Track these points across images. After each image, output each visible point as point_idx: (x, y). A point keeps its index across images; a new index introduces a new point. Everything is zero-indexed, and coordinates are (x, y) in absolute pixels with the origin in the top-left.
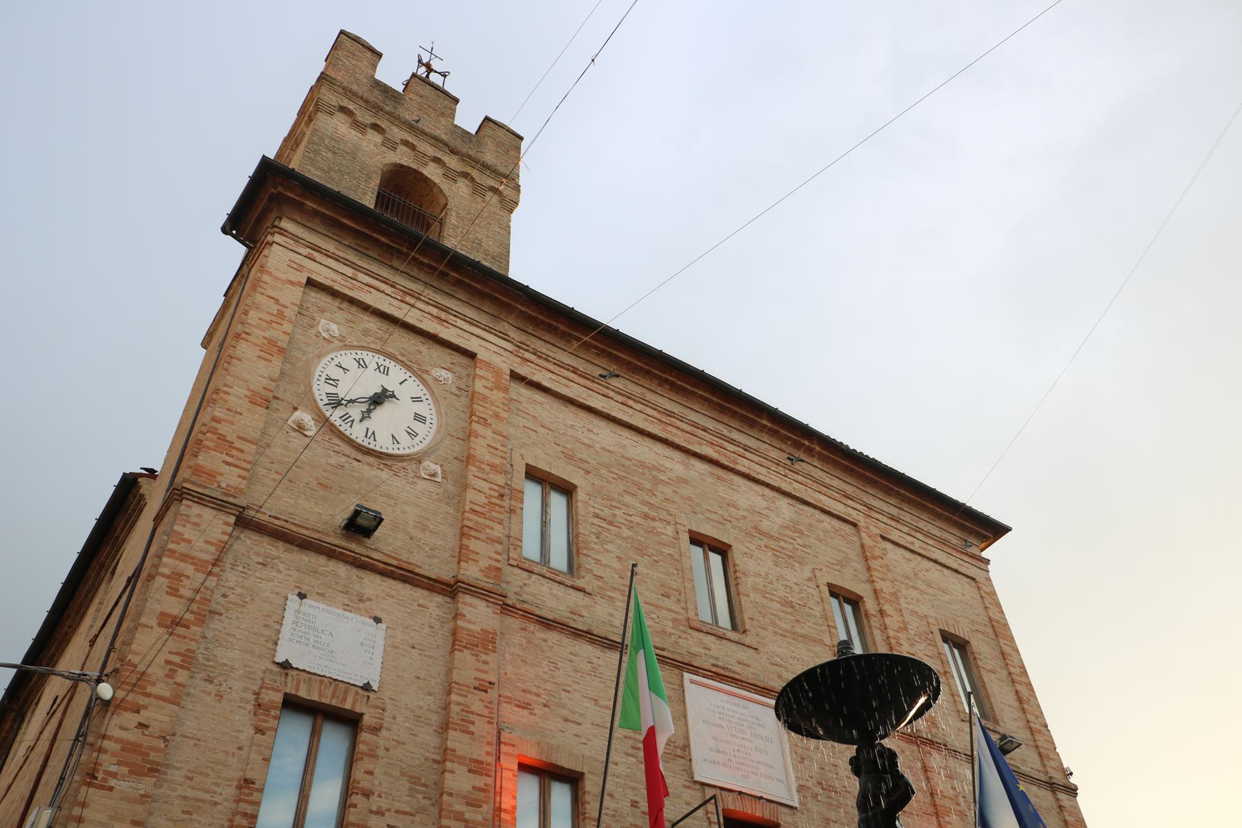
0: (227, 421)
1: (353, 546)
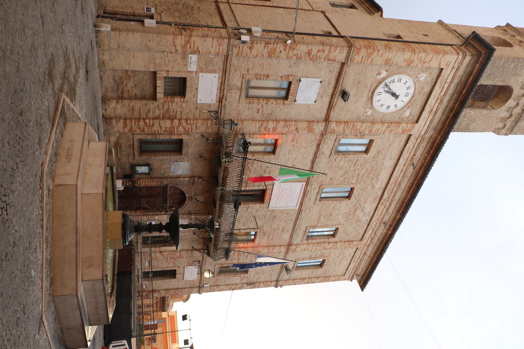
1: (338, 93)
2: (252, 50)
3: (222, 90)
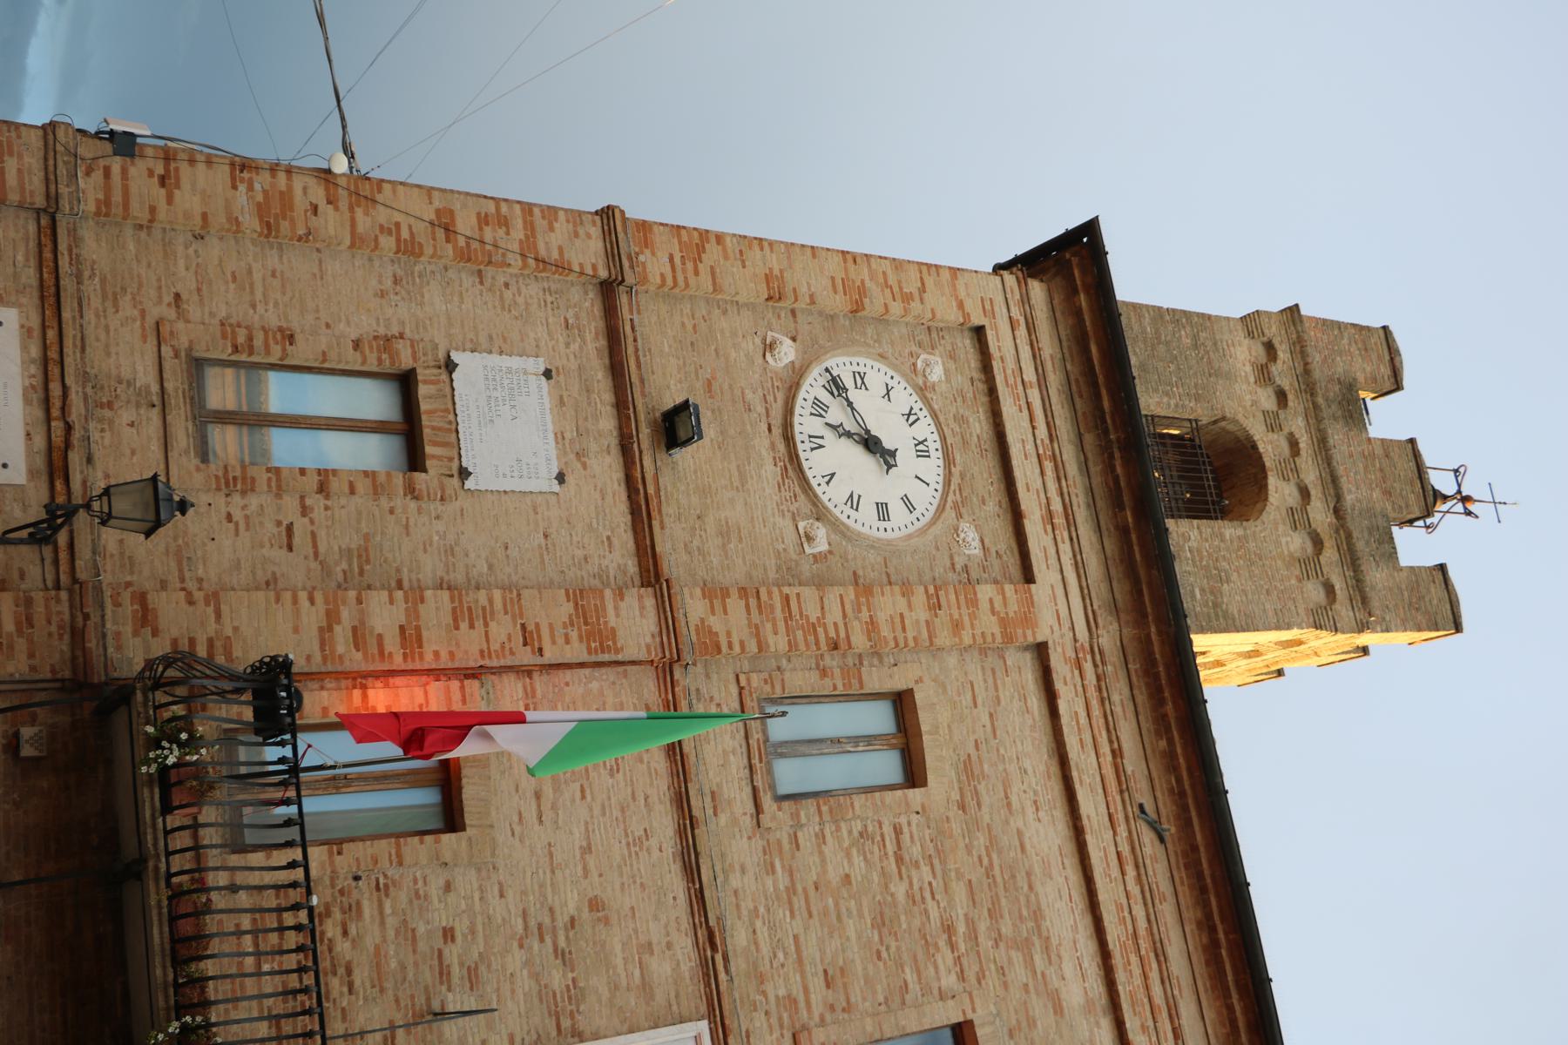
0: (724, 250)
2: (177, 192)
3: (56, 403)
